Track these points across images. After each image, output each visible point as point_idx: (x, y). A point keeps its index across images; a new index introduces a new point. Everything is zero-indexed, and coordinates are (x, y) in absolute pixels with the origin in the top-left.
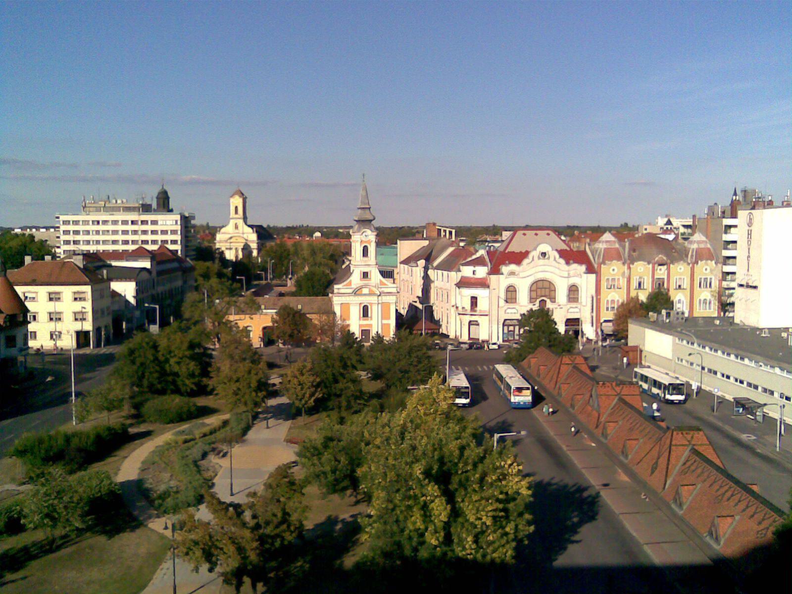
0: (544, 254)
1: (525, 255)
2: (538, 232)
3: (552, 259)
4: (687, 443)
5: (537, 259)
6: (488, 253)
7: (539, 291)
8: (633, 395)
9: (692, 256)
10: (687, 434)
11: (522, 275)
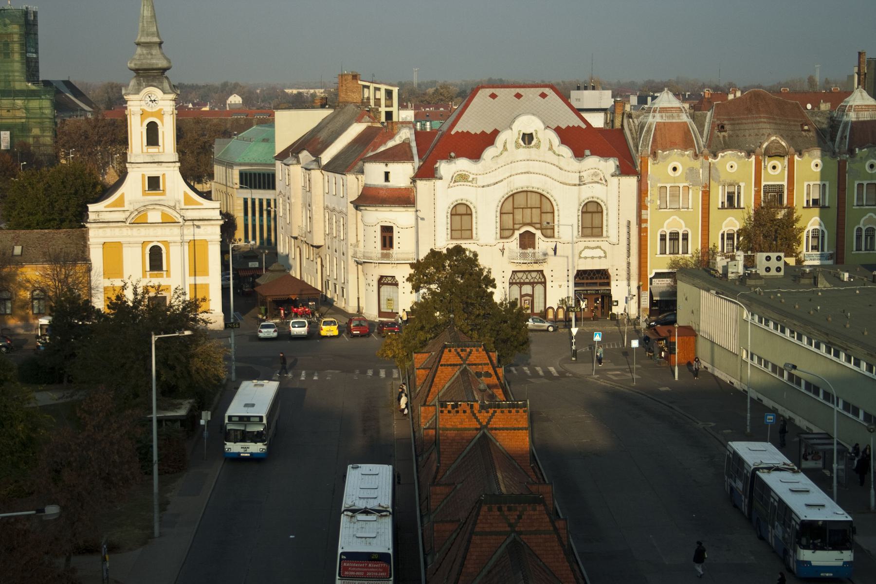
0: (528, 138)
1: (488, 139)
2: (520, 91)
3: (545, 146)
4: (508, 529)
9: (843, 138)
10: (510, 509)
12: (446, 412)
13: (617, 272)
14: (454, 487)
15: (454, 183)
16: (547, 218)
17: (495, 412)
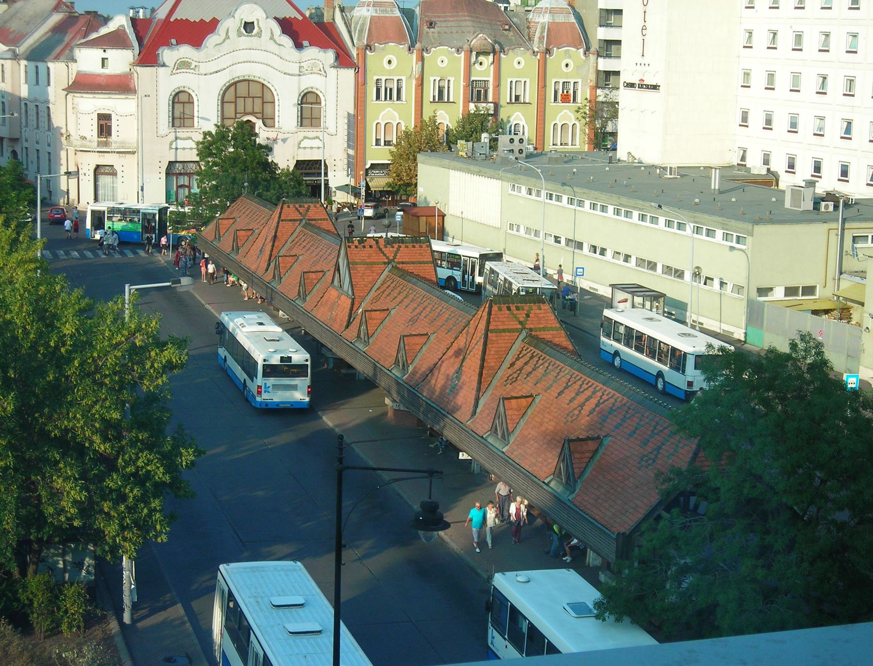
0: (248, 27)
3: (266, 35)
4: (520, 326)
5: (235, 33)
6: (134, 21)
7: (240, 102)
8: (420, 263)
9: (541, 38)
10: (518, 308)
11: (203, 68)
12: (353, 247)
13: (335, 163)
14: (388, 312)
15: (177, 70)
16: (268, 107)
17: (400, 247)
